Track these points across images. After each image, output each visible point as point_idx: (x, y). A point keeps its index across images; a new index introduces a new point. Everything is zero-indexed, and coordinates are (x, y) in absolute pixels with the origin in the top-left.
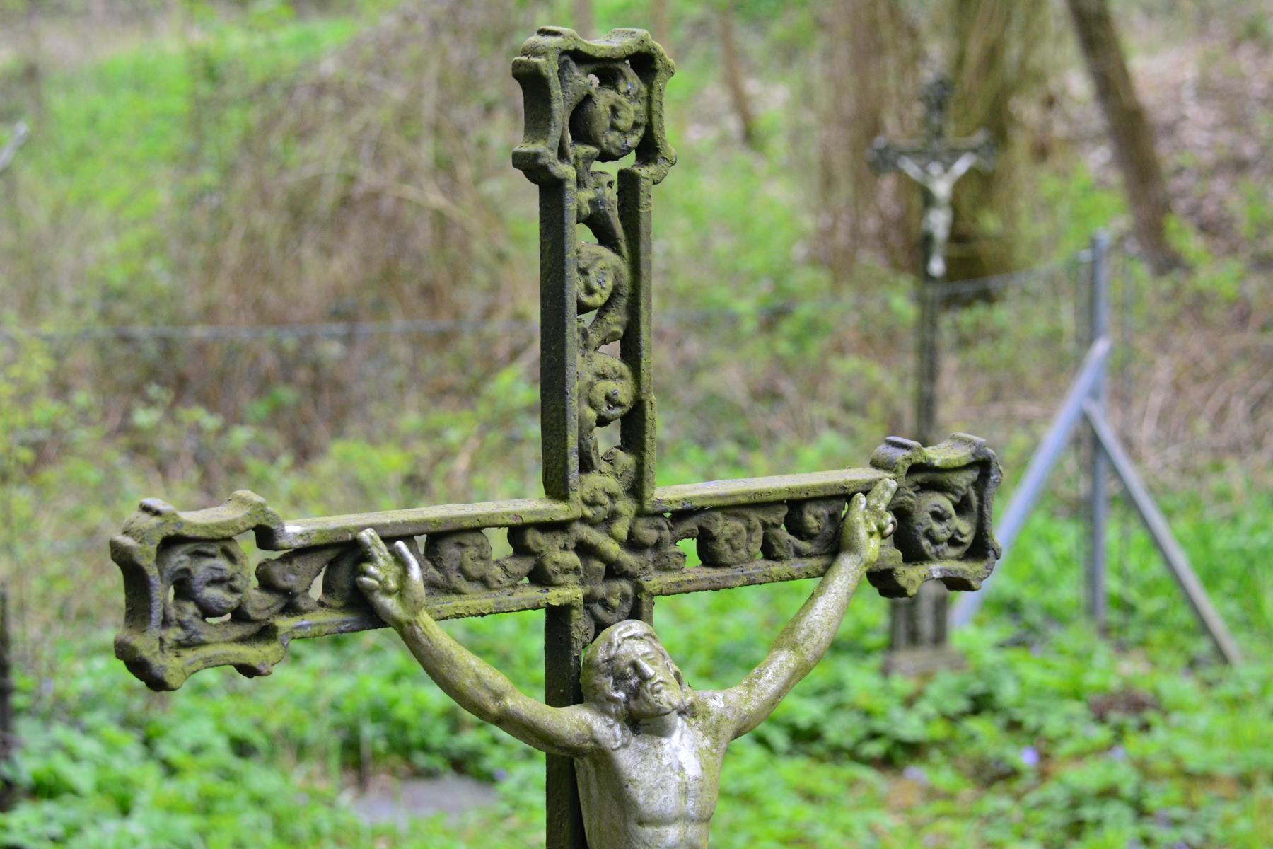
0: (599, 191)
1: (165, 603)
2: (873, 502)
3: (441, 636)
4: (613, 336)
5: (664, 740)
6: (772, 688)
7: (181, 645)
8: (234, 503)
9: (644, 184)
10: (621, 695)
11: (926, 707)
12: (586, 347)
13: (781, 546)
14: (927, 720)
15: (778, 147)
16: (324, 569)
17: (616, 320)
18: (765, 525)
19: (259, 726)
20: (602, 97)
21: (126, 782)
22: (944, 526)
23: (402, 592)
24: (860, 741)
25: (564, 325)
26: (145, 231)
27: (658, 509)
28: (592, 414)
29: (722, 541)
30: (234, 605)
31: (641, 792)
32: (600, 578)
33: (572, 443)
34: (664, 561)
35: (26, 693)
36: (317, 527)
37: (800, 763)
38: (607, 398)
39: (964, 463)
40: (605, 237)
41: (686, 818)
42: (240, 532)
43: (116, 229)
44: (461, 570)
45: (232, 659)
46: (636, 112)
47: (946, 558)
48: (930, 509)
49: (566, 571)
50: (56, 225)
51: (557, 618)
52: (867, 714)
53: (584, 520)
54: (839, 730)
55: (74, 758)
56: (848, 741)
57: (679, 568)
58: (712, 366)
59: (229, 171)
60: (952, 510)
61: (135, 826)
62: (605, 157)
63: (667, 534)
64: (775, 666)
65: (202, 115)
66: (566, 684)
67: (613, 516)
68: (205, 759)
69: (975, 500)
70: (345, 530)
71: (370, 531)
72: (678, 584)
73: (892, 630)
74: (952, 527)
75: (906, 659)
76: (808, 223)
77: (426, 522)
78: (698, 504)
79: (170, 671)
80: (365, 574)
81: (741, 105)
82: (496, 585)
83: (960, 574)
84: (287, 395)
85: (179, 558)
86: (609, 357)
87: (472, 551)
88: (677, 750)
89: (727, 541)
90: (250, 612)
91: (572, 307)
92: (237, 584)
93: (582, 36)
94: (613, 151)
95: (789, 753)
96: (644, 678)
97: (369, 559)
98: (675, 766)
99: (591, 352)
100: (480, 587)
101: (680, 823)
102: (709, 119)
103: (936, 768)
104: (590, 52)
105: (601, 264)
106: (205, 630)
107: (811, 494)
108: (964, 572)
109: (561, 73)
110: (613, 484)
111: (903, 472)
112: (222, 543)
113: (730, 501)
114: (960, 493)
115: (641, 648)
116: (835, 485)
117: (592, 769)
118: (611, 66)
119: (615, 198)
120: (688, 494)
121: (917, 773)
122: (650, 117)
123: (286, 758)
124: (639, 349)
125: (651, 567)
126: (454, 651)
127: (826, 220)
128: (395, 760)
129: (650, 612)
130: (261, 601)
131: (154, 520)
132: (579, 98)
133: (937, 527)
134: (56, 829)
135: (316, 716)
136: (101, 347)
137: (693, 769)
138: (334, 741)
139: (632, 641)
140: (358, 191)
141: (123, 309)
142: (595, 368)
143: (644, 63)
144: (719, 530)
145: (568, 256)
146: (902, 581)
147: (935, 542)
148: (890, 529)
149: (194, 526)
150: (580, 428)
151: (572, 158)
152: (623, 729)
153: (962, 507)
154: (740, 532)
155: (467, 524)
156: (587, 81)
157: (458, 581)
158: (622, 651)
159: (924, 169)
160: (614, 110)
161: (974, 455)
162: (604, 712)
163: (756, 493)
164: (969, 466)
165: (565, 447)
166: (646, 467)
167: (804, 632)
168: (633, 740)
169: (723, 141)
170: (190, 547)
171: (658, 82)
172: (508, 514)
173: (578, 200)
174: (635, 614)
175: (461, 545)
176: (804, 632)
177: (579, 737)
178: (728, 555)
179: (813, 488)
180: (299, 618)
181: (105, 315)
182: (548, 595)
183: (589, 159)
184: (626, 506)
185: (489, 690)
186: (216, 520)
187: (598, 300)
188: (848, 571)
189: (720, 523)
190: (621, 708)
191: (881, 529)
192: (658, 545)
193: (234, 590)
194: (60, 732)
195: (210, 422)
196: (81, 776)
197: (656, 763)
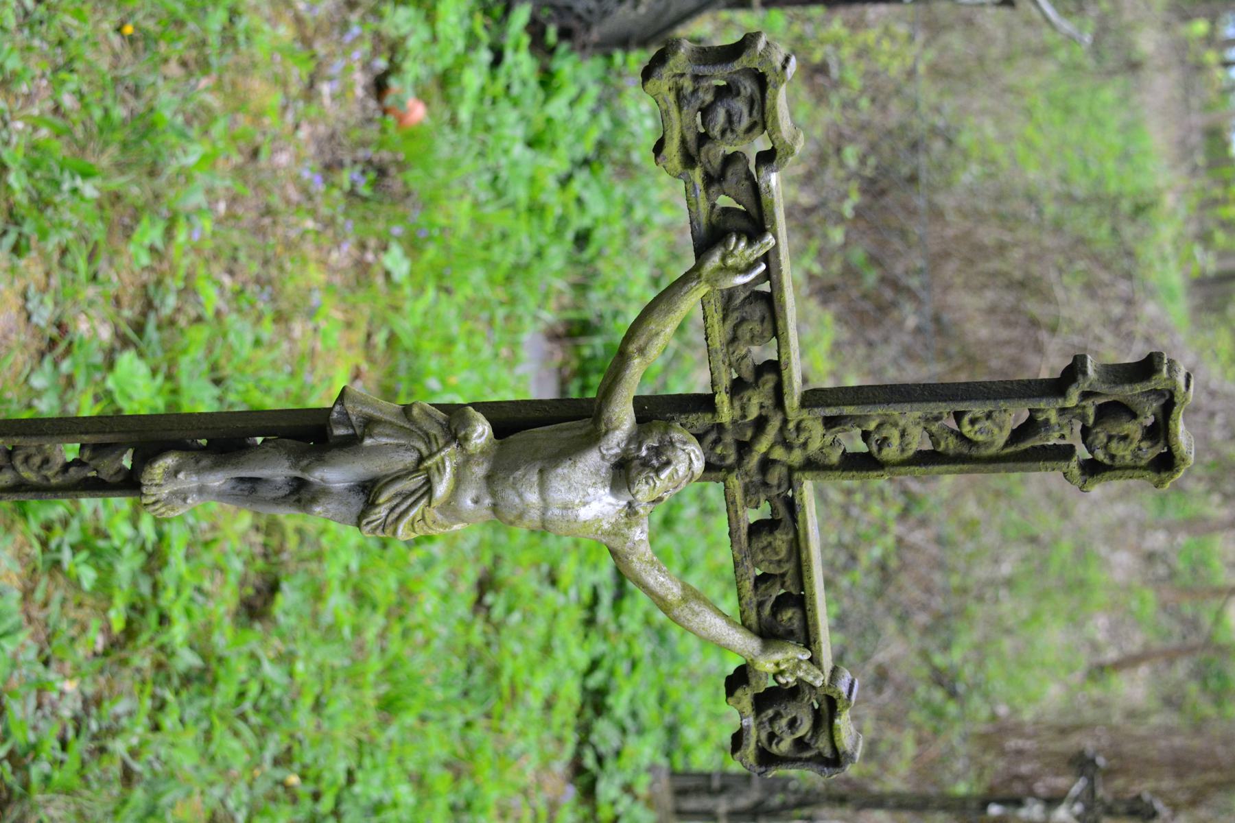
0: (1057, 428)
1: (712, 77)
2: (804, 666)
3: (690, 304)
4: (936, 443)
5: (607, 490)
6: (651, 581)
7: (679, 93)
8: (793, 131)
9: (1063, 464)
10: (644, 453)
11: (625, 802)
12: (927, 420)
13: (766, 589)
14: (614, 803)
15: (1095, 691)
16: (741, 207)
17: (950, 445)
18: (783, 575)
19: (600, 253)
20: (1135, 428)
21: (554, 146)
22: (785, 729)
23: (725, 269)
24: (594, 747)
25: (945, 401)
26: (1005, 163)
27: (795, 484)
28: (872, 426)
29: (770, 539)
30: (711, 133)
31: (566, 471)
32: (737, 437)
33: (848, 410)
34: (753, 490)
35: (625, 62)
36: (776, 199)
37: (576, 698)
38: (885, 439)
39: (838, 744)
40: (1019, 434)
41: (545, 509)
42: (770, 136)
43: (1006, 138)
44: (743, 320)
45: (668, 133)
46: (1123, 457)
47: (758, 731)
48: (799, 716)
49: (743, 408)
50: (1007, 90)
51: (705, 403)
52: (618, 754)
53: (785, 421)
54: (605, 732)
55: (573, 103)
56: (594, 738)
57: (747, 504)
58: (903, 632)
59: (1058, 227)
60: (798, 735)
61: (518, 150)
62: (1086, 432)
63: (775, 492)
64: (669, 584)
65: (1104, 203)
66: (655, 412)
67: (789, 447)
68: (573, 207)
69: (807, 755)
70: (773, 222)
71: (773, 242)
72: (734, 502)
73: (687, 774)
74: (784, 735)
75: (664, 785)
76: (1028, 715)
77: (781, 289)
78: (800, 518)
79: (658, 83)
80: (738, 240)
81: (1128, 663)
82: (731, 350)
83: (745, 742)
84: (871, 277)
85: (748, 87)
86: (919, 441)
87: (758, 328)
88: (600, 500)
89: (770, 544)
90: (706, 147)
91: (960, 407)
92: (729, 135)
93: (1186, 410)
94: (1091, 438)
95: (584, 689)
96: (658, 471)
97: (750, 243)
98: (587, 499)
99: (922, 424)
100: (729, 337)
101: (542, 504)
102: (1114, 630)
103: (574, 811)
104: (1173, 416)
105: (996, 430)
106: (691, 110)
107: (809, 614)
108: (748, 746)
109: (1154, 391)
110: (814, 446)
111: (828, 692)
112: (762, 120)
113: (802, 545)
114: (813, 742)
115: (682, 468)
116: (817, 634)
117: (583, 432)
118: (1162, 434)
119: (1051, 443)
120: (807, 510)
121: (570, 793)
122: (1120, 468)
123: (575, 275)
124: (926, 464)
125: (747, 480)
126: (677, 314)
127: (1029, 729)
128: (575, 364)
129: (711, 480)
130: (715, 155)
131: (778, 65)
132: (1134, 408)
133: (784, 722)
134: (516, 89)
135: (609, 298)
136: (904, 127)
137: (585, 513)
138: (589, 314)
139: (687, 461)
140: (1044, 335)
141: (938, 146)
142: (910, 429)
143: (1166, 463)
144: (779, 536)
145: (1002, 403)
146: (739, 693)
147: (772, 720)
148: (782, 680)
149: (774, 98)
150: (860, 417)
151: (1084, 403)
152: (616, 455)
153: (800, 744)
154: (777, 554)
155: (780, 323)
156: (1149, 414)
157: (734, 317)
158: (680, 453)
159: (1076, 799)
160: (1124, 438)
161: (844, 753)
162: (630, 440)
163: (809, 567)
164: (834, 748)
165: (844, 405)
166: (829, 473)
167: (696, 608)
168: (608, 464)
169: (1095, 647)
170: (758, 95)
171: (1150, 475)
172: (789, 358)
173: (1049, 410)
174: (709, 467)
175: (762, 320)
176: (696, 608)
177: (610, 419)
178: (758, 545)
179: (815, 615)
180: (702, 187)
181: (934, 131)
182: (723, 393)
183: (1083, 417)
184: (797, 457)
185: (647, 344)
186: (780, 116)
187: (967, 429)
188: (744, 645)
189: (784, 537)
190: (633, 453)
191: (781, 673)
192: (765, 484)
193: (723, 133)
194: (593, 91)
195: (848, 209)
196: (558, 107)
197: (589, 482)
